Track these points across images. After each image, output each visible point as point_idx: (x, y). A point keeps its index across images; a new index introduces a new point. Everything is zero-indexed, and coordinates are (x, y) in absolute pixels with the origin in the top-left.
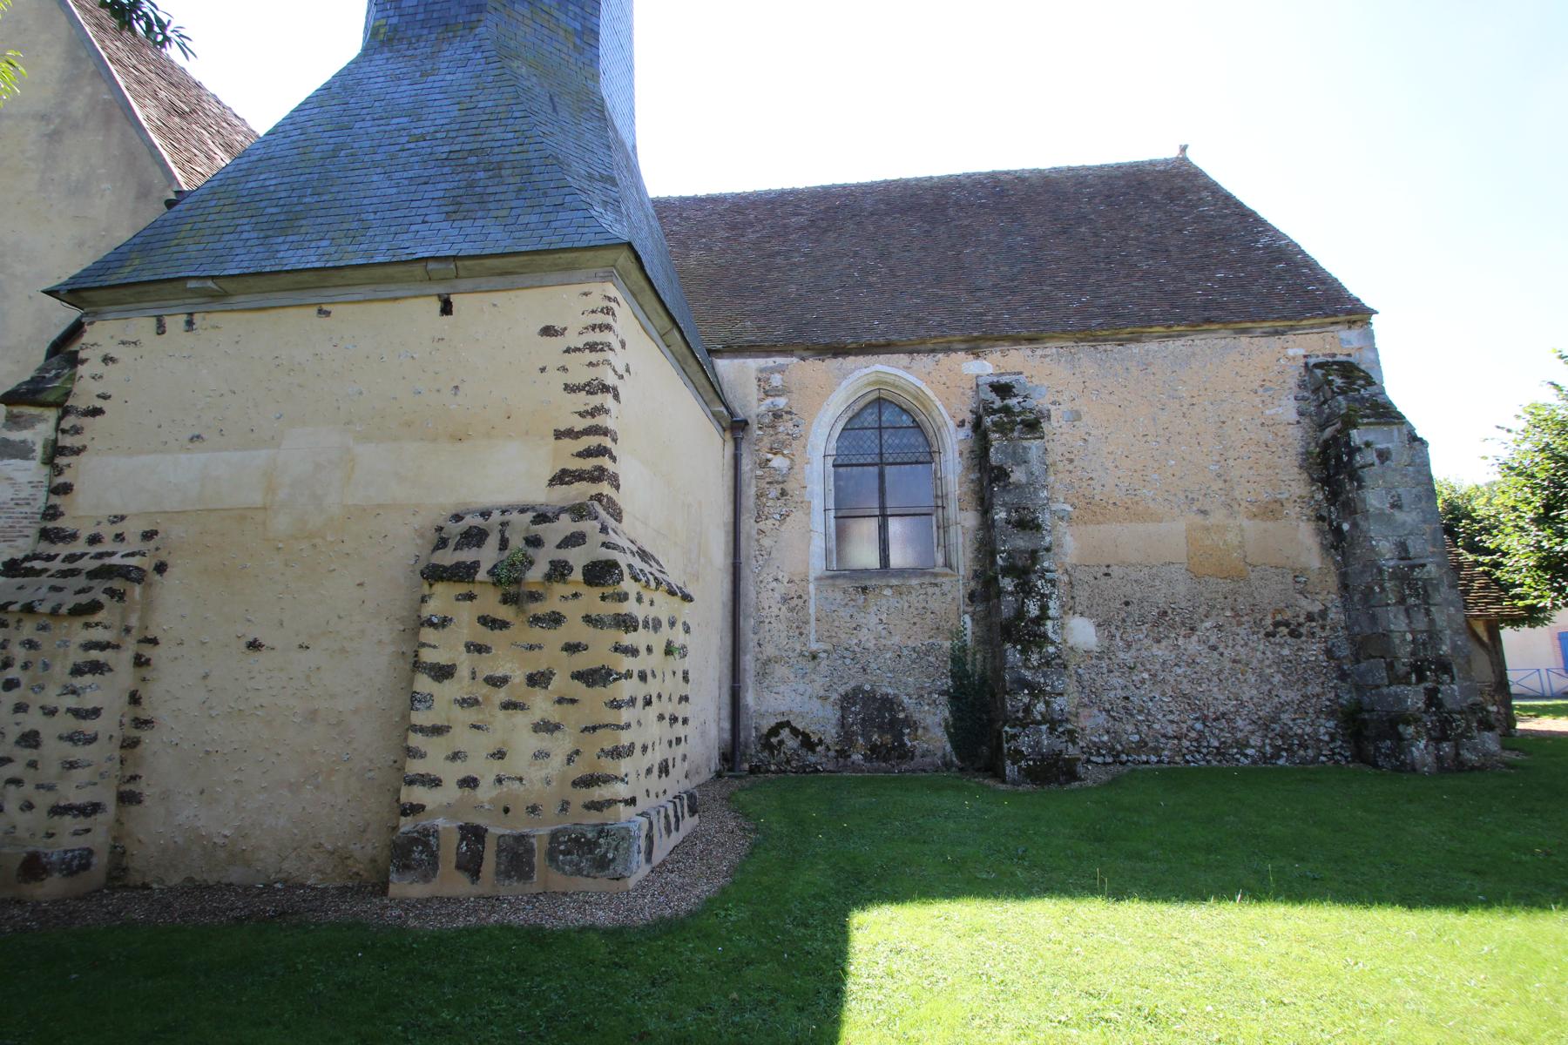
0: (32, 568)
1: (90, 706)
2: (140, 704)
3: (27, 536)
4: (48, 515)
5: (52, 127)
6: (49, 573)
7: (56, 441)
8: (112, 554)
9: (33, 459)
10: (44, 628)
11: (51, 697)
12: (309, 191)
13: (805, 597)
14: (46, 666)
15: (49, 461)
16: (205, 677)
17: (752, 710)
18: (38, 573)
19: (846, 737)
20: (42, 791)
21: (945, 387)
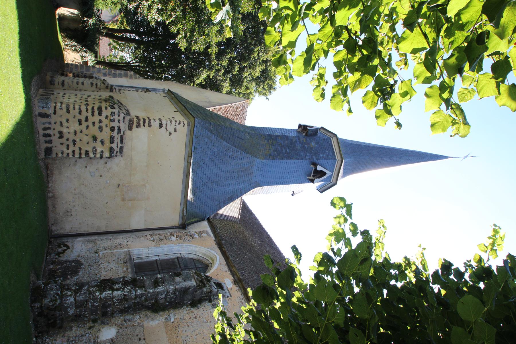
13: (121, 249)
17: (75, 240)
19: (61, 263)
21: (217, 274)
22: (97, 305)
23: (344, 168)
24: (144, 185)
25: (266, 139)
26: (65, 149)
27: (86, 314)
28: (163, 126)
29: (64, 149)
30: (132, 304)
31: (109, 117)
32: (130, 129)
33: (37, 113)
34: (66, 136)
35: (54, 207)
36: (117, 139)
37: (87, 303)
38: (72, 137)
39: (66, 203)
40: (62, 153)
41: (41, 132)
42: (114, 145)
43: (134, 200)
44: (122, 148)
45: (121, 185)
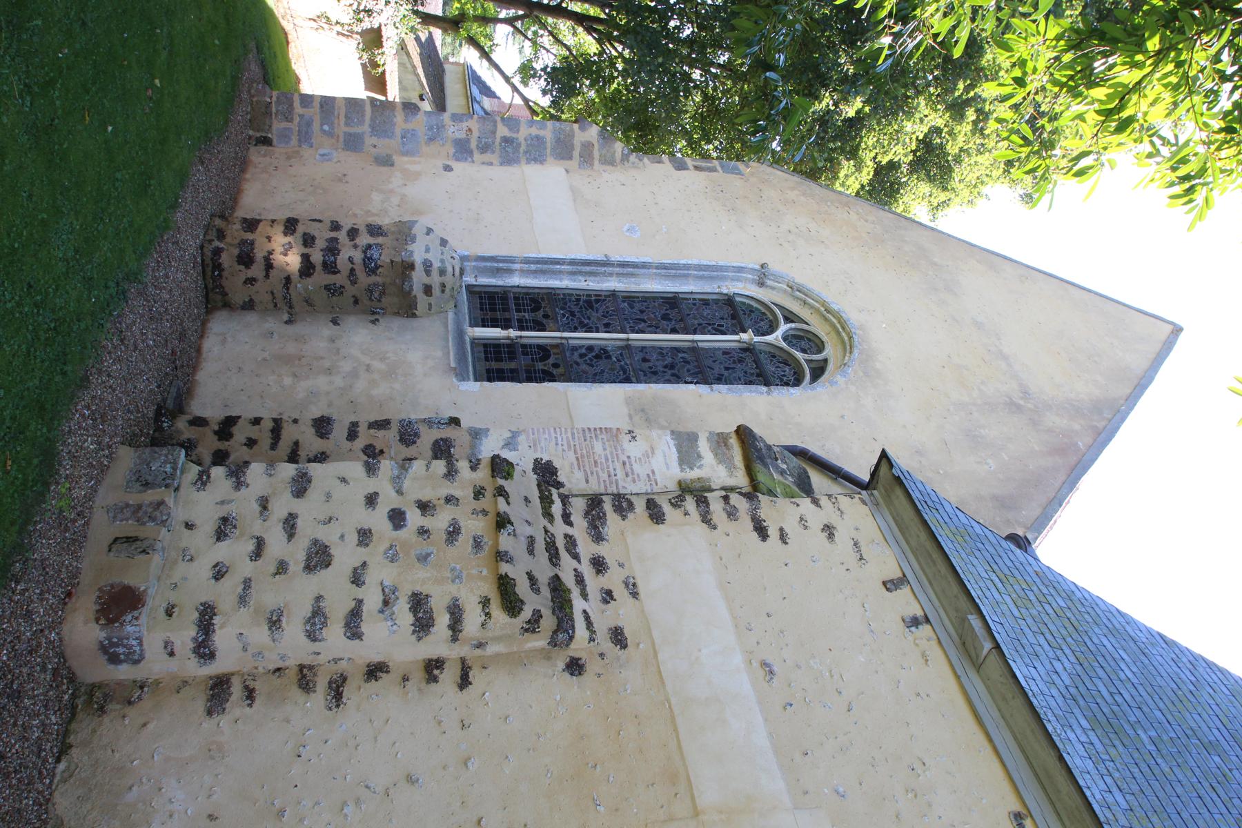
0: (552, 502)
1: (364, 628)
2: (368, 680)
3: (587, 481)
4: (620, 503)
5: (1022, 402)
6: (549, 526)
7: (710, 490)
8: (584, 595)
9: (682, 470)
10: (477, 544)
11: (380, 573)
12: (1153, 733)
14: (423, 558)
15: (685, 489)
16: (411, 780)
18: (548, 515)
20: (240, 589)
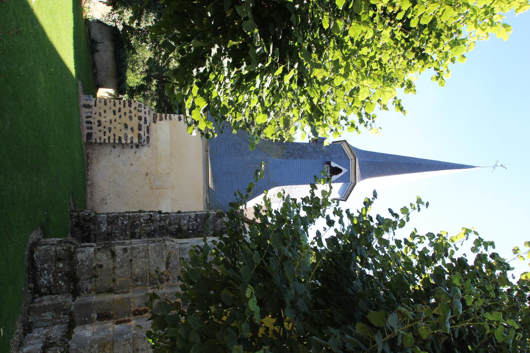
22: (126, 223)
23: (360, 169)
24: (169, 173)
25: (278, 145)
26: (102, 136)
27: (117, 233)
28: (181, 119)
29: (102, 135)
30: (157, 227)
31: (137, 108)
32: (155, 122)
33: (82, 104)
34: (103, 124)
35: (92, 195)
36: (144, 128)
37: (117, 219)
38: (108, 125)
39: (102, 191)
40: (100, 139)
41: (85, 120)
42: (142, 133)
43: (161, 188)
44: (148, 138)
45: (149, 174)
